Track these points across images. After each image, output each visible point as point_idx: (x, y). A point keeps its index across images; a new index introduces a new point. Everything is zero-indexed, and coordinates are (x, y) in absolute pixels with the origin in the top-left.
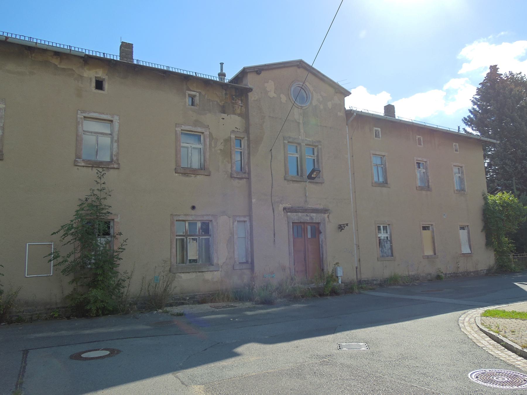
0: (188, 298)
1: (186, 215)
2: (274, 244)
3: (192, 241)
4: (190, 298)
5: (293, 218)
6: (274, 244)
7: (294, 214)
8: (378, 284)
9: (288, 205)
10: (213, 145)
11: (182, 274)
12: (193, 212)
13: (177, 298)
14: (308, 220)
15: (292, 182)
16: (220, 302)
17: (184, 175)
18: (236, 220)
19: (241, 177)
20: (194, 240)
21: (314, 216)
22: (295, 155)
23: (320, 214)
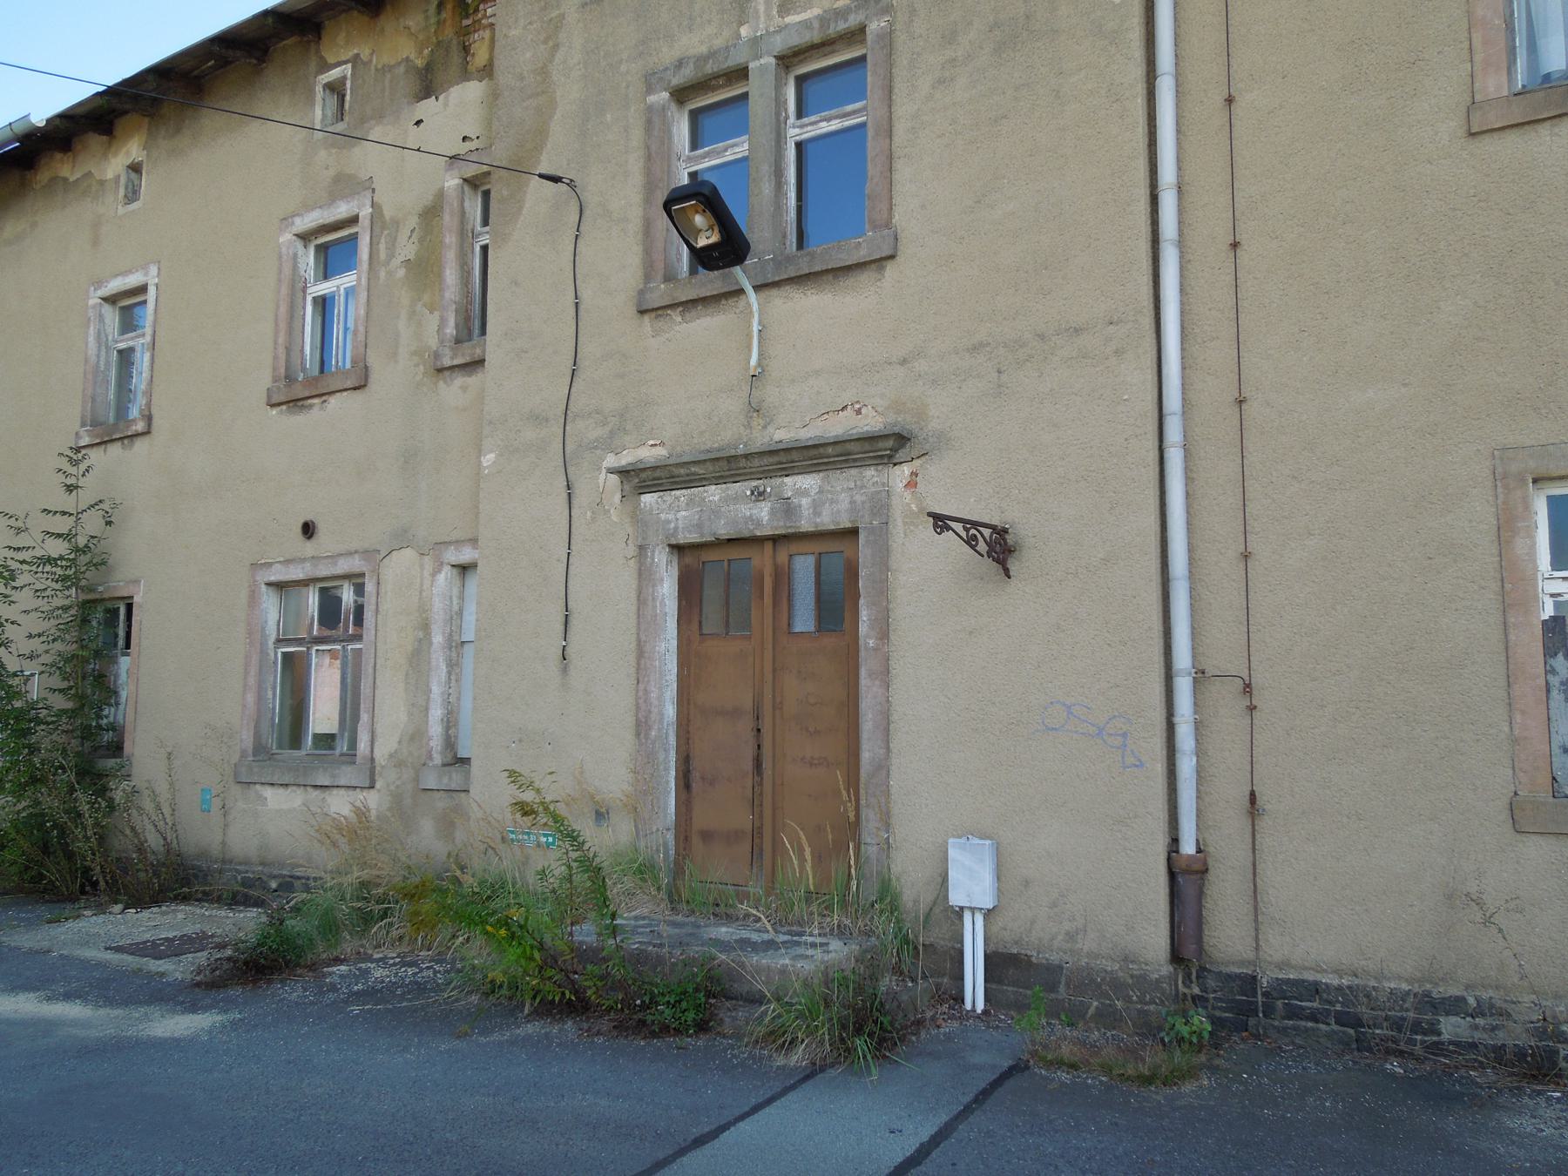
0: (274, 885)
1: (288, 562)
2: (565, 670)
3: (327, 660)
4: (280, 885)
5: (669, 522)
6: (565, 670)
7: (677, 498)
8: (1499, 1050)
9: (648, 454)
10: (383, 256)
11: (267, 787)
12: (309, 548)
13: (247, 875)
14: (759, 523)
15: (682, 314)
16: (1326, 984)
17: (296, 405)
18: (442, 563)
19: (468, 359)
20: (335, 659)
21: (803, 493)
22: (737, 150)
23: (854, 472)
